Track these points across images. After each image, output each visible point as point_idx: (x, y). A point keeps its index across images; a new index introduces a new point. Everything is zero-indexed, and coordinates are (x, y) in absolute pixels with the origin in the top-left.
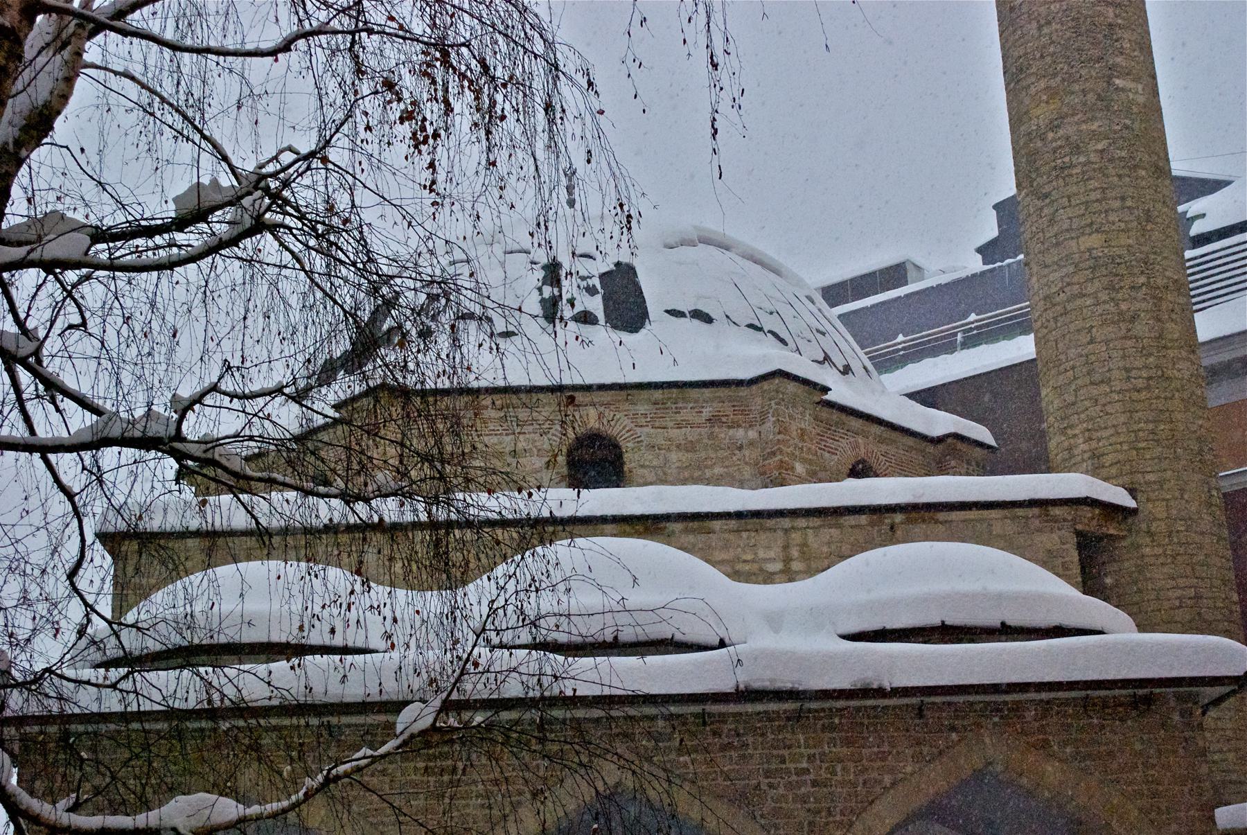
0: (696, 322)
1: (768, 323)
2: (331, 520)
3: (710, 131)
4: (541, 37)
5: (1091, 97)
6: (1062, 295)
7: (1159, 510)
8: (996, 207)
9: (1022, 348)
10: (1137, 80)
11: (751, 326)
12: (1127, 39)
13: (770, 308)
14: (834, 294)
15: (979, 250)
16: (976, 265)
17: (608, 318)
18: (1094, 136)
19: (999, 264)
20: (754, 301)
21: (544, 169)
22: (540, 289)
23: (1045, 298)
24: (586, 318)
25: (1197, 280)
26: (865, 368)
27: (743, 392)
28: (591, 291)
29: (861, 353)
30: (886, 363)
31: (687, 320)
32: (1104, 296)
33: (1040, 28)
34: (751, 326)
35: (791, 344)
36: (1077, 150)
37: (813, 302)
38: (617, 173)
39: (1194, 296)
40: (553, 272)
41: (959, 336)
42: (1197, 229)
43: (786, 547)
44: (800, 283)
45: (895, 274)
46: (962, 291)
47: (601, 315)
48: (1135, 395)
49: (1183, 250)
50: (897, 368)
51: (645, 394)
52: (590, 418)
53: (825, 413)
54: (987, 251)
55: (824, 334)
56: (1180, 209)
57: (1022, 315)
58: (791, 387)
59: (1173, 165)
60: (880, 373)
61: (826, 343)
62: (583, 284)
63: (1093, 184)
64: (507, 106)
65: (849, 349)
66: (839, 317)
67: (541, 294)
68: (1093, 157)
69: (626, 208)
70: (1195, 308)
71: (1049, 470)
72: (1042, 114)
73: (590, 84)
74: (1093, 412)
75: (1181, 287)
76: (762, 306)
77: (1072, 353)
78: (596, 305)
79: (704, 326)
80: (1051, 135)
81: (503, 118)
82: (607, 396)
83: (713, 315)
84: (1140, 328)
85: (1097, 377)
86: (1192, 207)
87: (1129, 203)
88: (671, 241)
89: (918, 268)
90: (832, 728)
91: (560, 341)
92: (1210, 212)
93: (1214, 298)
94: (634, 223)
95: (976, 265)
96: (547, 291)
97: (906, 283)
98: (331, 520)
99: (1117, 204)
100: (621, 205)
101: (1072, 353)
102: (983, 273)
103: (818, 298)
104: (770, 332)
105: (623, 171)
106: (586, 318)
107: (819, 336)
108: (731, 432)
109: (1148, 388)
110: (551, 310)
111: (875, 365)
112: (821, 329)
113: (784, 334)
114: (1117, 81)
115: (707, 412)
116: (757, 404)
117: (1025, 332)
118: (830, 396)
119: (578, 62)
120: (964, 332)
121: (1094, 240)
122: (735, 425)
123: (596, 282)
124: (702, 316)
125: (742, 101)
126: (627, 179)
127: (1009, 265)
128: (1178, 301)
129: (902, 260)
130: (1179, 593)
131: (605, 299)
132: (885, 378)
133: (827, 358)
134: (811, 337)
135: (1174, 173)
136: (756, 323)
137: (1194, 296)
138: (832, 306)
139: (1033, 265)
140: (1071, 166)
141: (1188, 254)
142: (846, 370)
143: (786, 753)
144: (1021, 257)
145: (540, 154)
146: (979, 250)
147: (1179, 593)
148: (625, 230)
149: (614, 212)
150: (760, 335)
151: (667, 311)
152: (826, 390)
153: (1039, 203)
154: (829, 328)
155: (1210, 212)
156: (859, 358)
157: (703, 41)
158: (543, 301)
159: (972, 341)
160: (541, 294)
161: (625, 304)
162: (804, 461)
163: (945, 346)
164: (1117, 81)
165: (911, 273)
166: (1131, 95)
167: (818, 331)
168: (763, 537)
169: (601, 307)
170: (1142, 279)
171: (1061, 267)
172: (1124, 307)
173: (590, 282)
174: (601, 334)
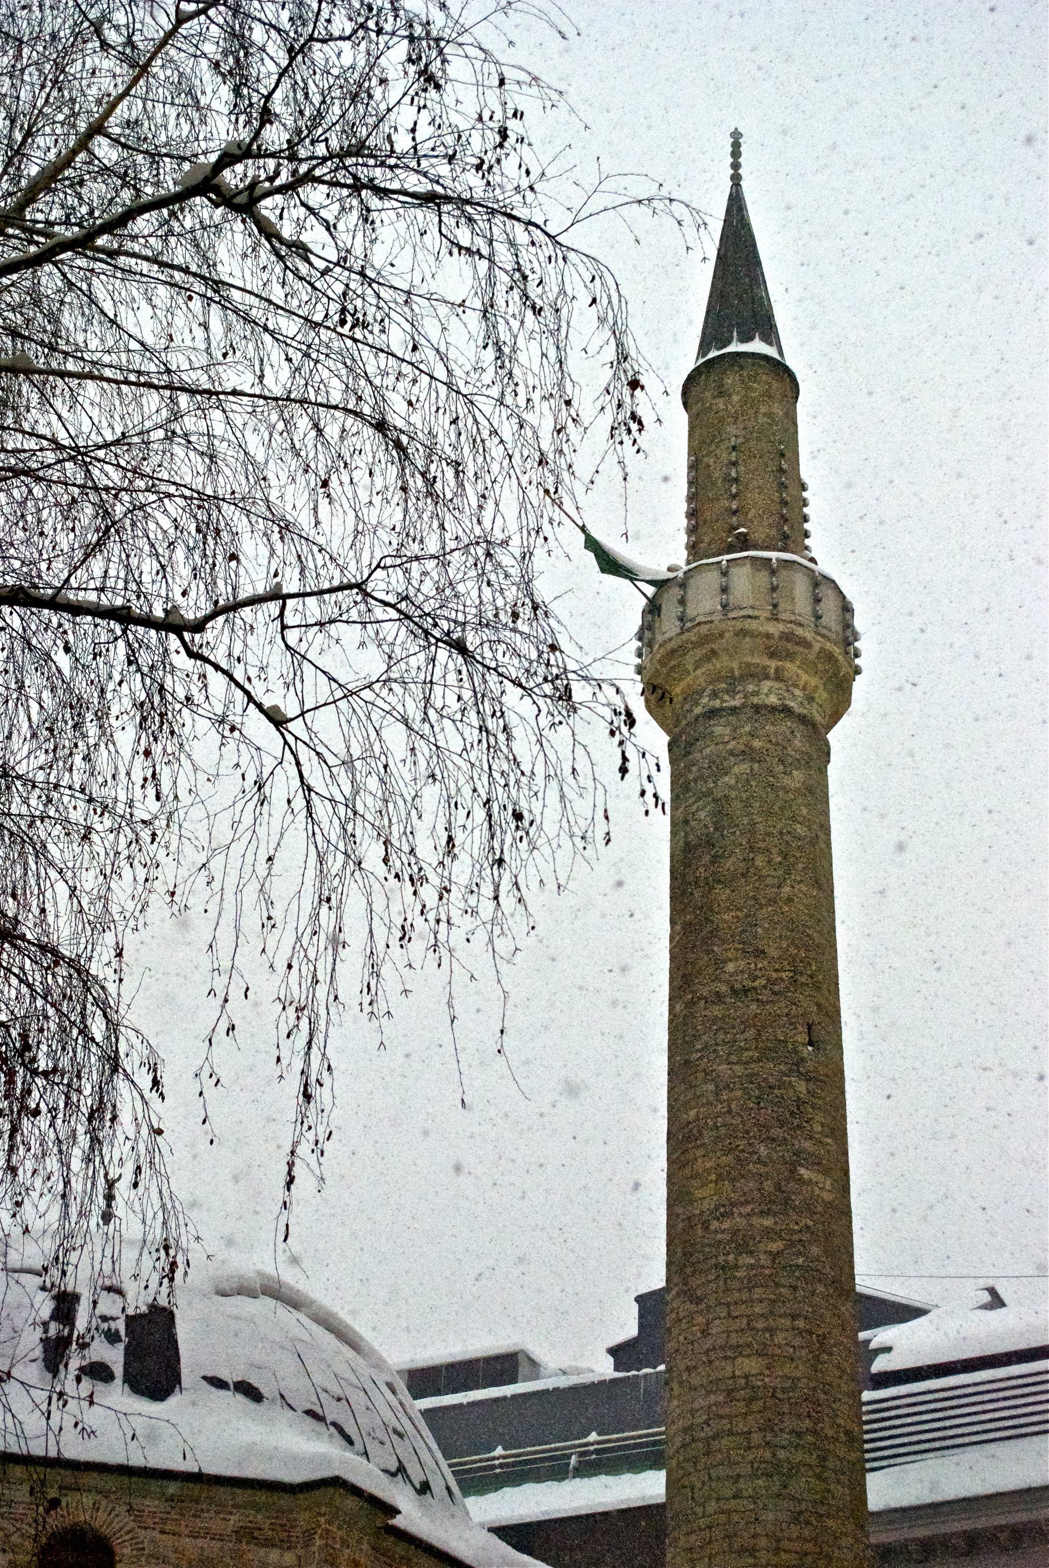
0: (240, 1398)
1: (333, 1412)
3: (283, 1177)
4: (105, 1015)
5: (768, 1185)
6: (706, 1429)
8: (639, 1299)
9: (649, 1487)
10: (826, 1172)
11: (310, 1413)
13: (337, 1391)
14: (424, 1380)
15: (613, 1351)
16: (605, 1368)
17: (128, 1379)
18: (768, 1234)
19: (634, 1373)
20: (318, 1378)
21: (77, 1186)
22: (45, 1325)
23: (686, 1430)
24: (99, 1372)
25: (875, 1431)
26: (448, 1489)
27: (285, 1501)
28: (112, 1337)
29: (443, 1463)
30: (478, 1482)
31: (230, 1393)
33: (717, 1093)
34: (310, 1413)
35: (358, 1445)
37: (394, 1392)
38: (169, 1206)
40: (65, 1305)
41: (573, 1460)
42: (880, 1364)
44: (379, 1364)
45: (505, 1366)
46: (581, 1401)
47: (118, 1370)
49: (860, 1392)
50: (489, 1491)
51: (154, 1485)
52: (82, 1509)
53: (389, 1542)
54: (620, 1353)
55: (400, 1435)
56: (863, 1335)
57: (655, 1443)
58: (351, 1503)
59: (858, 1280)
60: (465, 1496)
61: (403, 1450)
62: (105, 1326)
64: (42, 1105)
65: (431, 1460)
66: (427, 1413)
67: (46, 1331)
68: (764, 1259)
69: (172, 1252)
70: (868, 1466)
72: (706, 1197)
73: (156, 1082)
75: (854, 1440)
76: (329, 1388)
77: (712, 1507)
78: (114, 1356)
79: (252, 1405)
80: (715, 1225)
81: (36, 1112)
82: (110, 1482)
83: (264, 1390)
84: (799, 1485)
86: (880, 1336)
87: (800, 1323)
88: (226, 1286)
89: (533, 1363)
91: (55, 1421)
92: (901, 1345)
93: (897, 1456)
94: (179, 1274)
95: (605, 1368)
96: (54, 1328)
97: (513, 1381)
99: (787, 1322)
100: (167, 1248)
101: (712, 1507)
102: (613, 1381)
103: (401, 1386)
104: (335, 1424)
105: (177, 1204)
106: (99, 1372)
107: (394, 1437)
108: (262, 1552)
110: (54, 1353)
111: (459, 1483)
112: (400, 1429)
113: (351, 1430)
114: (802, 1171)
115: (235, 1520)
116: (303, 1519)
117: (656, 1466)
118: (398, 1521)
119: (146, 1052)
120: (582, 1454)
121: (750, 1365)
122: (269, 1543)
123: (120, 1326)
124: (249, 1391)
125: (328, 1146)
126: (181, 1216)
127: (646, 1376)
128: (849, 1458)
129: (511, 1349)
131: (126, 1349)
132: (472, 1503)
133: (401, 1470)
134: (386, 1439)
135: (858, 1289)
136: (317, 1409)
137: (868, 1451)
138: (415, 1397)
139: (675, 1385)
140: (736, 1267)
141: (867, 1395)
142: (424, 1489)
144: (662, 1367)
145: (76, 1164)
146: (613, 1351)
148: (166, 1280)
149: (155, 1255)
150: (321, 1427)
151: (204, 1378)
152: (394, 1511)
153: (693, 1307)
154: (408, 1426)
155: (901, 1345)
156: (440, 1470)
157: (298, 1065)
158: (45, 1341)
159: (594, 1465)
160: (46, 1331)
161: (152, 1358)
163: (555, 1470)
164: (802, 1171)
165: (524, 1369)
166: (817, 1191)
167: (395, 1431)
169: (121, 1359)
170: (807, 1423)
171: (709, 1393)
172: (782, 1454)
173: (113, 1325)
174: (117, 1395)
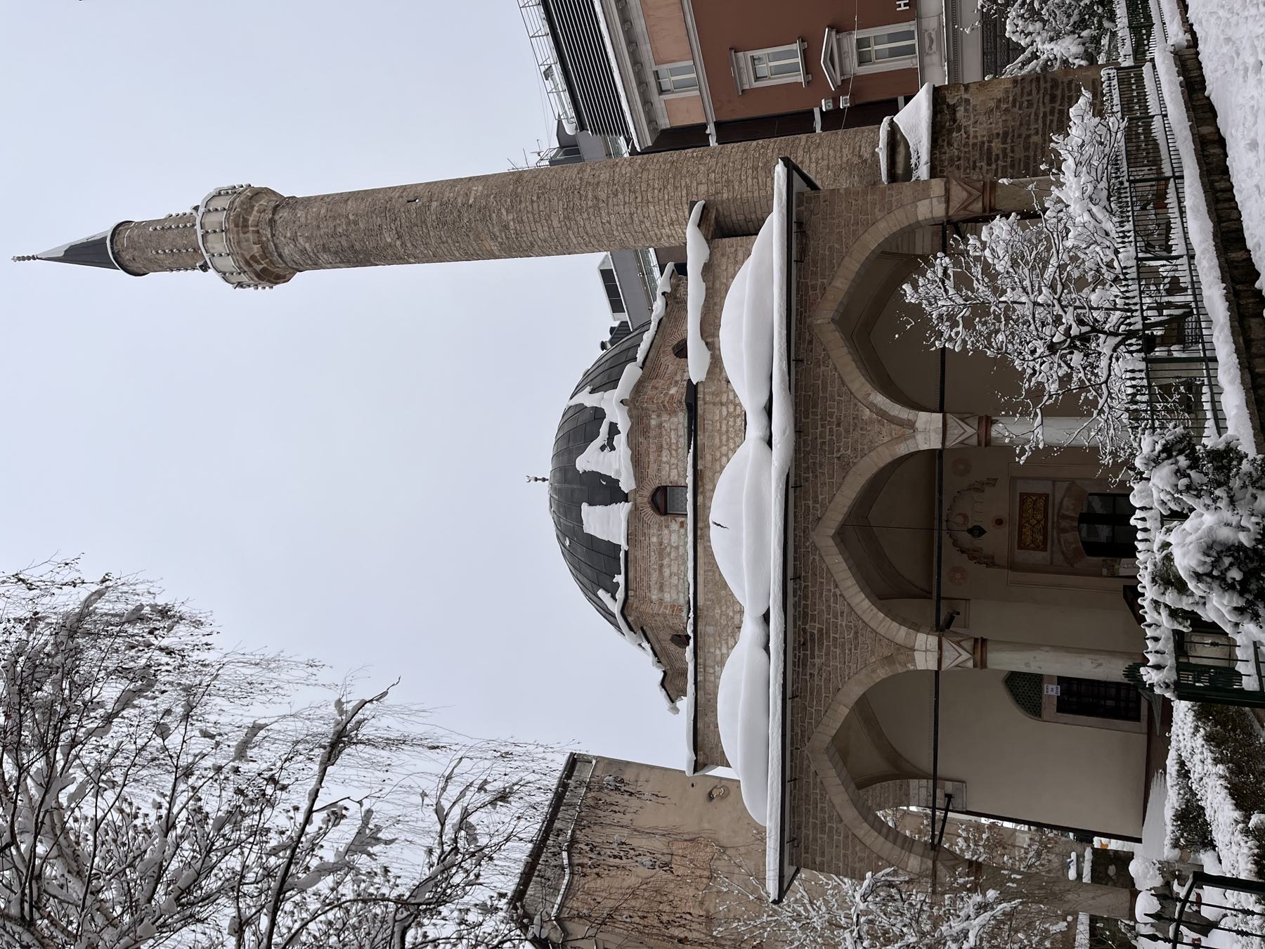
2: (1221, 777)
7: (703, 188)
12: (448, 195)
32: (585, 216)
36: (506, 227)
39: (1080, 875)
43: (714, 404)
48: (639, 200)
63: (525, 218)
68: (510, 217)
71: (686, 265)
74: (648, 224)
85: (628, 221)
90: (807, 411)
98: (1221, 777)
99: (535, 205)
109: (635, 192)
130: (750, 180)
137: (1080, 875)
143: (819, 441)
147: (750, 180)
162: (669, 389)
168: (708, 416)
